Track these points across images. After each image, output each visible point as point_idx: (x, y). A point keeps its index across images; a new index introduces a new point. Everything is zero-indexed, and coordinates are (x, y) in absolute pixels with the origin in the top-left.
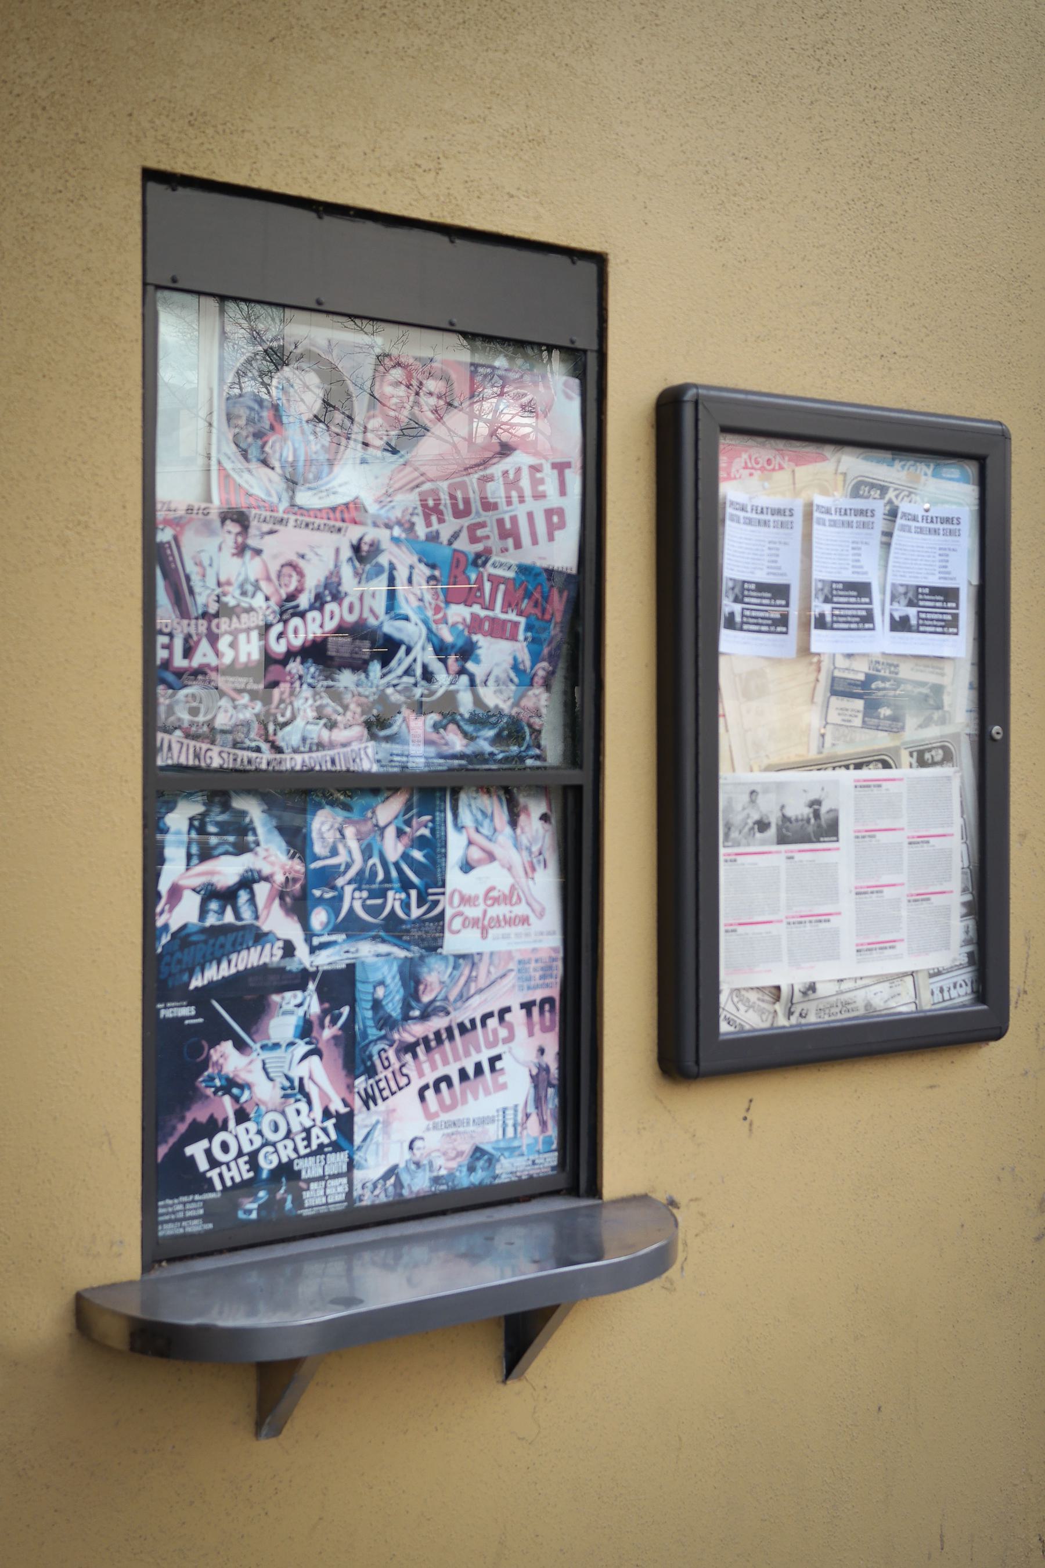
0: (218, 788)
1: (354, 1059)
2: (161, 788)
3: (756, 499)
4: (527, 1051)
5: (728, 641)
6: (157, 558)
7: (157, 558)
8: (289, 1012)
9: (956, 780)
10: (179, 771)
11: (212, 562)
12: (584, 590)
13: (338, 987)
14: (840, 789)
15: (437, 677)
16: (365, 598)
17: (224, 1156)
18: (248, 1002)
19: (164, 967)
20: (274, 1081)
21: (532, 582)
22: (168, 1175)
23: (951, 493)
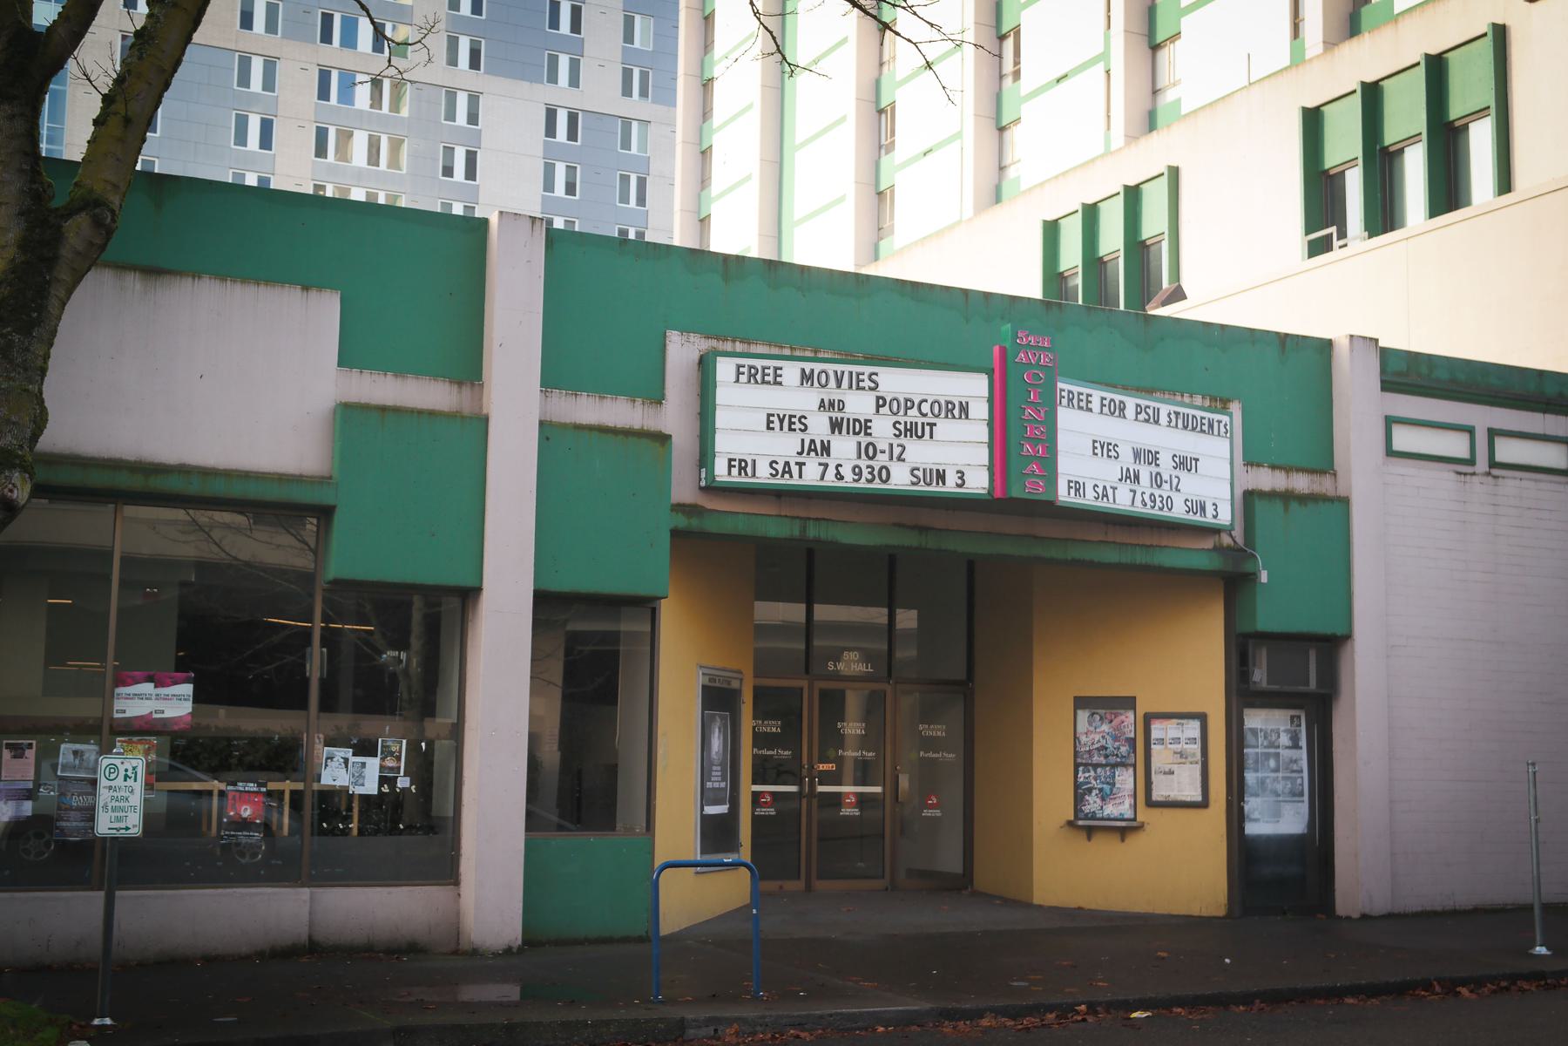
0: (1086, 765)
1: (1103, 799)
2: (1077, 766)
3: (1157, 730)
4: (1128, 802)
5: (306, 890)
6: (1075, 737)
7: (1075, 737)
8: (1095, 792)
9: (1198, 767)
10: (243, 13)
11: (1083, 739)
12: (1134, 740)
13: (1101, 790)
14: (1175, 768)
15: (742, 850)
16: (1103, 742)
17: (1087, 809)
18: (1090, 790)
19: (1077, 786)
20: (1092, 803)
21: (1128, 740)
22: (1077, 810)
23: (1196, 724)
